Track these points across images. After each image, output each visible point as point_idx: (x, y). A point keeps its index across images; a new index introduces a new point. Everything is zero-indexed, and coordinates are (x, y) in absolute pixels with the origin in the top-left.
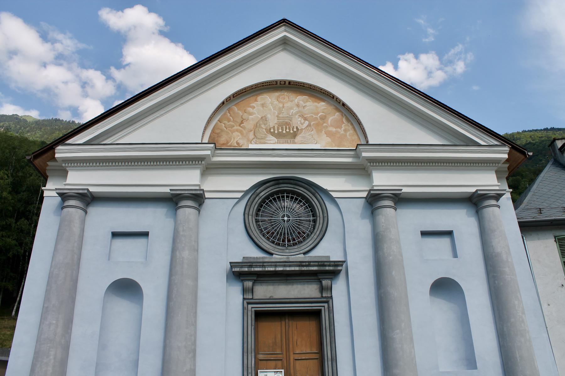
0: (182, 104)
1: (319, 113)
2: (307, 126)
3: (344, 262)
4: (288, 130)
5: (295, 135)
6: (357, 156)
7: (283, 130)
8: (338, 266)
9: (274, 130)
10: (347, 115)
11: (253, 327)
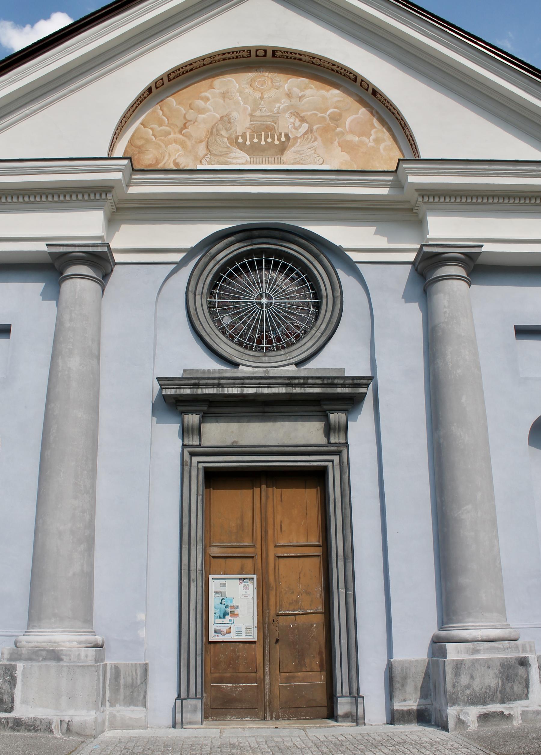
0: (72, 91)
1: (327, 109)
2: (306, 133)
3: (371, 378)
4: (269, 140)
5: (282, 149)
6: (398, 184)
7: (260, 139)
8: (359, 385)
9: (245, 140)
10: (380, 112)
11: (200, 497)
